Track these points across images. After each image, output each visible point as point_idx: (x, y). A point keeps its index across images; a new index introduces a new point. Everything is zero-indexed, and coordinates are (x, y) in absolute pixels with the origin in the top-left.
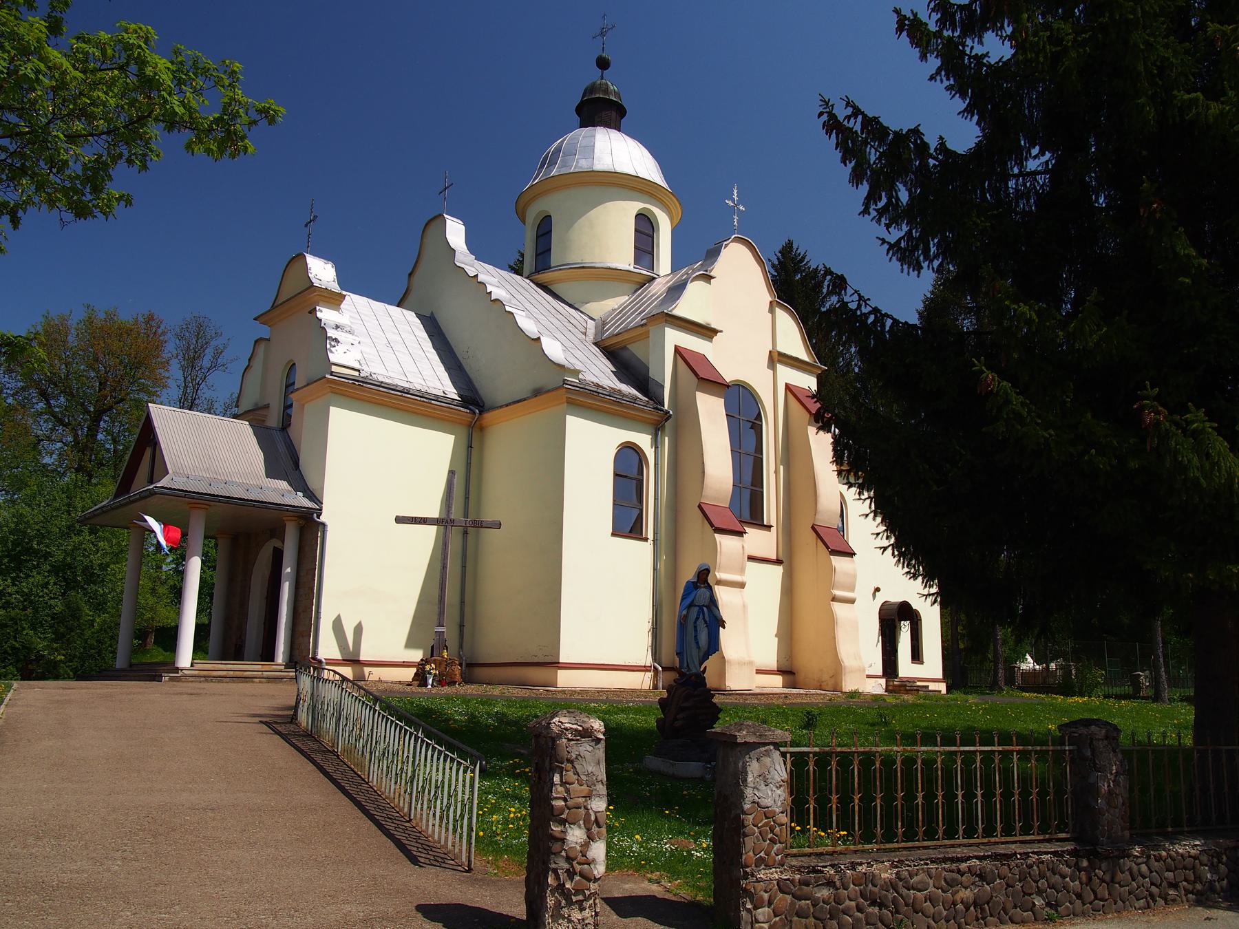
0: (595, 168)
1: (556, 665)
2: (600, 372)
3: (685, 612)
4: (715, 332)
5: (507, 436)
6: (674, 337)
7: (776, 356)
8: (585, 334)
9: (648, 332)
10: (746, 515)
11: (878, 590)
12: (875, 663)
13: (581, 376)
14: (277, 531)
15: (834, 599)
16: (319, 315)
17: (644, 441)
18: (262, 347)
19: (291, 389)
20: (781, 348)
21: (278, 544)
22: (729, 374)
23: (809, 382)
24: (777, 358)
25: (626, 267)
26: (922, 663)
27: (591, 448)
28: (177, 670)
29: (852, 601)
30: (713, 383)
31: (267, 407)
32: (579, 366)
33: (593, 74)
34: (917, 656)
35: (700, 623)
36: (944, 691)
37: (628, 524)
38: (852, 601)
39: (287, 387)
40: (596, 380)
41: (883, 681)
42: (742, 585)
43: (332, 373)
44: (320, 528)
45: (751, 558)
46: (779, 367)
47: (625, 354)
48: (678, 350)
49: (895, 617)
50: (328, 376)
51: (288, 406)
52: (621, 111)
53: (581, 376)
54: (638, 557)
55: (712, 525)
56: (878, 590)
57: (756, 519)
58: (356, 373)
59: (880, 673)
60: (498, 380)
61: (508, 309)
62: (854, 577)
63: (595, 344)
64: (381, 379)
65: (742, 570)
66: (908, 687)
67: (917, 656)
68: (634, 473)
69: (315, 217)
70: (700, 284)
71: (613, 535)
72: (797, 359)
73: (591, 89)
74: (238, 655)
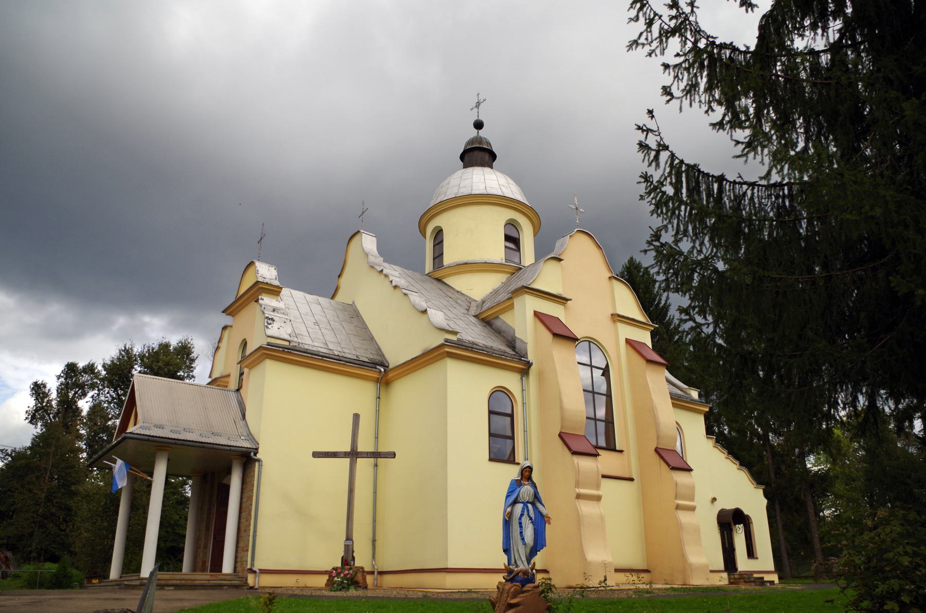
0: (474, 192)
2: (473, 333)
3: (509, 509)
4: (567, 300)
11: (714, 500)
18: (226, 333)
23: (645, 338)
24: (618, 318)
25: (500, 261)
29: (693, 509)
30: (564, 336)
32: (457, 329)
33: (473, 133)
34: (751, 554)
35: (525, 520)
36: (777, 581)
37: (268, 344)
38: (693, 509)
40: (471, 339)
42: (598, 498)
44: (257, 464)
45: (604, 476)
47: (497, 323)
48: (537, 314)
49: (729, 521)
52: (493, 156)
55: (570, 449)
56: (714, 500)
57: (611, 446)
58: (287, 343)
59: (722, 567)
61: (404, 291)
64: (306, 347)
65: (598, 487)
66: (747, 577)
67: (751, 554)
70: (553, 264)
71: (491, 460)
73: (471, 141)
74: (204, 570)
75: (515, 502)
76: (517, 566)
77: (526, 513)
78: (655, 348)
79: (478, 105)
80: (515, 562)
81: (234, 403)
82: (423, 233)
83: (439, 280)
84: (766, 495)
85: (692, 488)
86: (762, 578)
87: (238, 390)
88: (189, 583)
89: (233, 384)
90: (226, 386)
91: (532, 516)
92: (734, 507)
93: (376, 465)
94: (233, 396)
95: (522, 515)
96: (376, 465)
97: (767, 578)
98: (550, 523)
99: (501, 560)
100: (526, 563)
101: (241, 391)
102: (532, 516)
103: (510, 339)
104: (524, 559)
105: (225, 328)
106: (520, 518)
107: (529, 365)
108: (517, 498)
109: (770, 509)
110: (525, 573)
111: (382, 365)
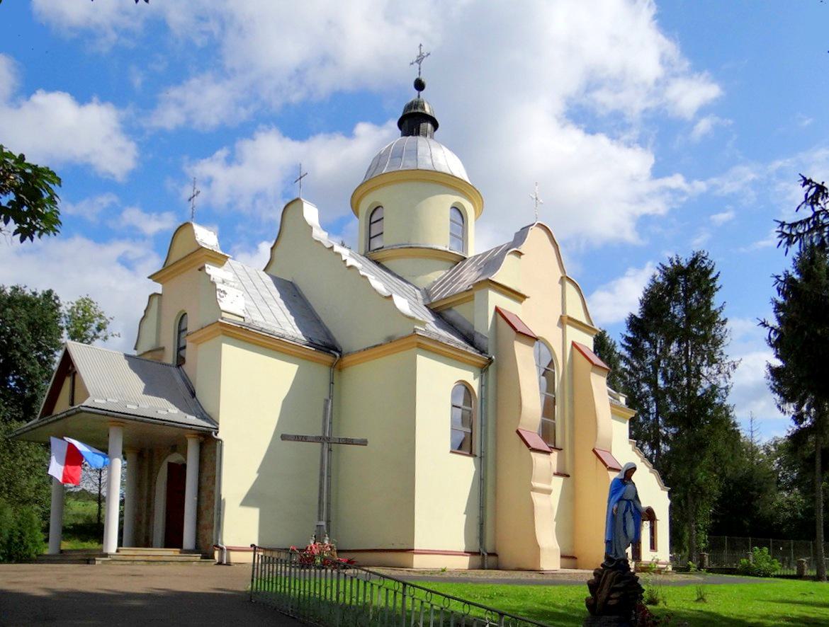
2: (431, 327)
4: (524, 297)
5: (366, 378)
6: (495, 299)
7: (566, 320)
8: (416, 298)
9: (473, 295)
14: (178, 445)
16: (208, 271)
17: (475, 384)
18: (155, 300)
19: (183, 335)
20: (570, 313)
21: (175, 458)
24: (565, 321)
25: (443, 248)
26: (657, 551)
27: (438, 383)
28: (106, 555)
33: (413, 95)
34: (653, 546)
39: (180, 332)
43: (222, 318)
46: (569, 329)
47: (451, 315)
50: (220, 320)
51: (181, 348)
54: (467, 466)
58: (242, 320)
61: (362, 273)
64: (261, 326)
65: (549, 481)
67: (653, 546)
69: (198, 192)
70: (513, 257)
71: (451, 452)
72: (580, 323)
73: (410, 106)
74: (148, 544)
77: (629, 511)
79: (420, 60)
84: (670, 496)
89: (170, 358)
95: (626, 511)
106: (624, 514)
109: (672, 509)
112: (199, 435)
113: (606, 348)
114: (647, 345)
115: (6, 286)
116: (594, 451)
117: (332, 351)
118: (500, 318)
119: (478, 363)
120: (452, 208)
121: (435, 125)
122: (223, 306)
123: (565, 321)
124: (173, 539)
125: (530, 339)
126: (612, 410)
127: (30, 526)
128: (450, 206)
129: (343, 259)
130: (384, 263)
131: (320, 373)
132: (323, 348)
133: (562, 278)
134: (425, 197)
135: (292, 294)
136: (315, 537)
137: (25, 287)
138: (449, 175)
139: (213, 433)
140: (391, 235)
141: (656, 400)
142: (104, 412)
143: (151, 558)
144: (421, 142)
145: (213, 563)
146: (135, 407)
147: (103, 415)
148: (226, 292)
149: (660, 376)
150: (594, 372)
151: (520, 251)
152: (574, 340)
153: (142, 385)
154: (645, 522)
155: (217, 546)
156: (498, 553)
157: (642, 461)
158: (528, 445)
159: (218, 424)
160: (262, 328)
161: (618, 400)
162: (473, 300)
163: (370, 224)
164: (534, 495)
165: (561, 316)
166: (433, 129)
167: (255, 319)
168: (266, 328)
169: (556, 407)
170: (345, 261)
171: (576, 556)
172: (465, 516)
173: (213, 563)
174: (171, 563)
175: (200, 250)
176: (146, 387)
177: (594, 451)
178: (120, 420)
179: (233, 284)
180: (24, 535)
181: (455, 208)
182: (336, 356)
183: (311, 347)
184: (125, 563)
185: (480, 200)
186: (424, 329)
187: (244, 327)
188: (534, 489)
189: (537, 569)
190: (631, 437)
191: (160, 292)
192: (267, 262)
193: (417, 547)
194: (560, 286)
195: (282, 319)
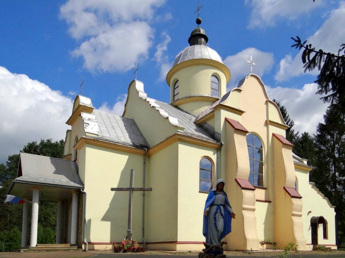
1: (176, 242)
3: (208, 209)
5: (159, 159)
6: (224, 114)
7: (268, 122)
10: (256, 184)
11: (310, 212)
12: (309, 240)
13: (185, 131)
15: (293, 215)
17: (214, 158)
18: (69, 133)
20: (271, 119)
22: (250, 129)
23: (282, 133)
24: (268, 123)
29: (300, 216)
31: (71, 154)
34: (325, 236)
35: (218, 216)
38: (300, 216)
41: (312, 246)
42: (254, 210)
44: (84, 195)
45: (257, 201)
46: (270, 126)
47: (206, 126)
48: (226, 120)
49: (317, 222)
53: (185, 131)
56: (310, 212)
57: (260, 185)
58: (97, 136)
59: (311, 242)
60: (154, 138)
62: (301, 206)
63: (194, 123)
64: (107, 138)
65: (254, 205)
66: (323, 249)
67: (325, 236)
68: (210, 169)
70: (236, 92)
71: (199, 192)
72: (277, 124)
75: (212, 205)
76: (212, 244)
77: (219, 211)
78: (287, 138)
80: (211, 241)
81: (73, 167)
82: (169, 84)
83: (176, 107)
84: (336, 211)
85: (301, 206)
86: (330, 248)
87: (75, 161)
88: (53, 249)
90: (70, 160)
91: (223, 213)
92: (320, 216)
93: (144, 195)
94: (73, 164)
95: (216, 213)
96: (144, 195)
97: (333, 248)
98: (234, 218)
99: (204, 239)
100: (218, 242)
101: (77, 161)
102: (223, 213)
103: (212, 133)
104: (217, 239)
105: (68, 131)
106: (215, 215)
107: (222, 145)
108: (213, 202)
109: (337, 217)
110: (217, 247)
111: (147, 147)
112: (77, 191)
113: (308, 141)
114: (329, 137)
115: (44, 140)
116: (284, 188)
117: (144, 148)
118: (227, 123)
119: (214, 147)
120: (212, 76)
121: (206, 39)
122: (86, 130)
123: (268, 123)
124: (64, 240)
125: (243, 132)
126: (295, 167)
127: (50, 235)
128: (211, 75)
129: (150, 104)
130: (180, 107)
131: (139, 160)
132: (139, 147)
133: (266, 101)
134: (197, 72)
135: (131, 124)
136: (126, 237)
137: (52, 139)
138: (210, 60)
139: (82, 190)
140: (182, 92)
141: (334, 164)
142: (68, 187)
143: (48, 249)
144: (197, 47)
145: (82, 250)
146: (43, 180)
147: (25, 184)
148: (89, 124)
149: (336, 151)
150: (236, 133)
151: (241, 89)
152: (274, 133)
153: (54, 169)
154: (320, 224)
155: (83, 242)
156: (227, 242)
157: (318, 193)
158: (240, 186)
159: (84, 185)
160: (107, 139)
161: (303, 162)
162: (214, 117)
163: (174, 89)
164: (245, 213)
165: (266, 121)
166: (205, 41)
167: (104, 135)
168: (109, 139)
169: (263, 166)
170: (151, 104)
171: (276, 243)
172: (264, 225)
173: (82, 250)
174: (59, 251)
175: (80, 106)
176: (55, 171)
177: (284, 188)
178: (34, 186)
179: (94, 120)
180: (47, 239)
181: (214, 76)
182: (145, 150)
183: (133, 147)
184: (35, 251)
185: (226, 68)
186: (183, 132)
187: (96, 139)
188: (244, 209)
189: (246, 250)
190: (310, 180)
191: (70, 129)
192: (124, 111)
193: (179, 240)
194: (265, 106)
195: (120, 134)
